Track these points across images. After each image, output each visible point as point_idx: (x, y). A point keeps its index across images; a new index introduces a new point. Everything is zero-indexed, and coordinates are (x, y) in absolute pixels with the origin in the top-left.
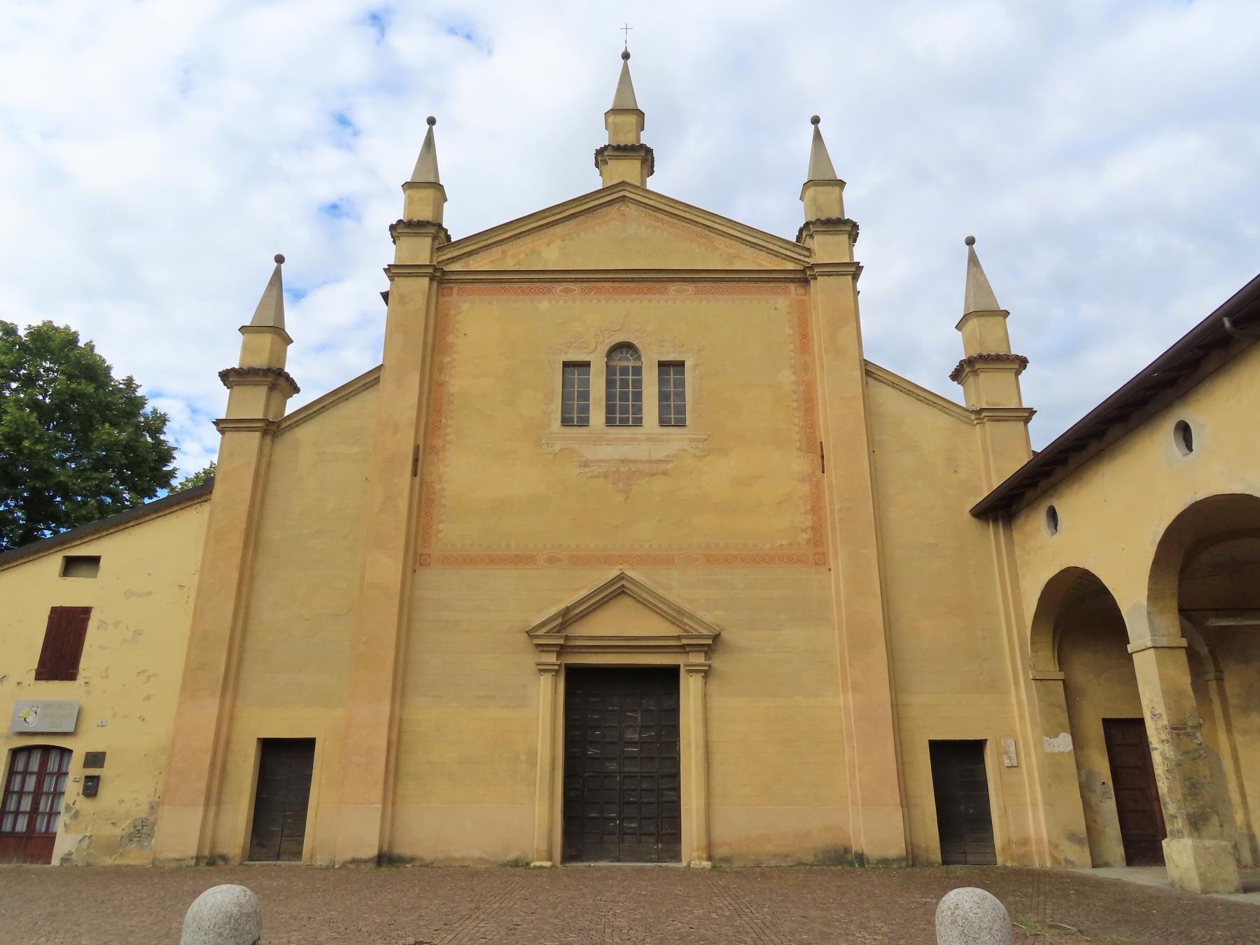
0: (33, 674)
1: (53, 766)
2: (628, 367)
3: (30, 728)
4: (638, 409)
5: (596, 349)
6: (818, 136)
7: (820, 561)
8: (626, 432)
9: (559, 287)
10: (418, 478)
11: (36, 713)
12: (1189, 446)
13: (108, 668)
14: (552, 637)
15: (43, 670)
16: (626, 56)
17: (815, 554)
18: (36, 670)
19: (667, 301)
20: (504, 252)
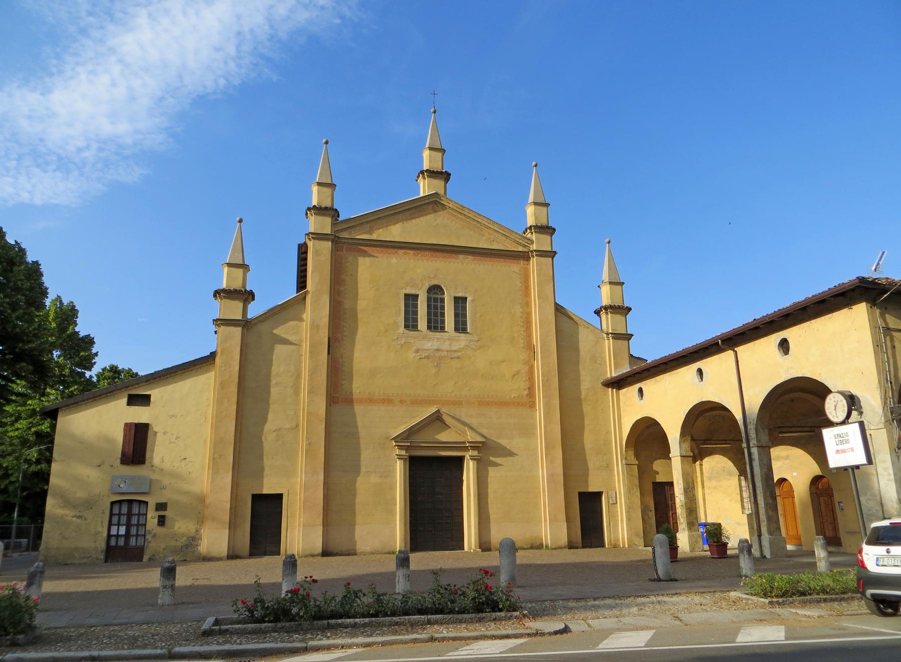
0: (119, 461)
1: (135, 510)
2: (438, 298)
3: (124, 490)
4: (443, 322)
5: (422, 287)
7: (532, 405)
8: (438, 335)
9: (401, 252)
10: (330, 355)
11: (125, 482)
12: (702, 379)
13: (163, 457)
14: (404, 442)
17: (530, 402)
18: (357, 472)
19: (458, 263)
20: (371, 227)
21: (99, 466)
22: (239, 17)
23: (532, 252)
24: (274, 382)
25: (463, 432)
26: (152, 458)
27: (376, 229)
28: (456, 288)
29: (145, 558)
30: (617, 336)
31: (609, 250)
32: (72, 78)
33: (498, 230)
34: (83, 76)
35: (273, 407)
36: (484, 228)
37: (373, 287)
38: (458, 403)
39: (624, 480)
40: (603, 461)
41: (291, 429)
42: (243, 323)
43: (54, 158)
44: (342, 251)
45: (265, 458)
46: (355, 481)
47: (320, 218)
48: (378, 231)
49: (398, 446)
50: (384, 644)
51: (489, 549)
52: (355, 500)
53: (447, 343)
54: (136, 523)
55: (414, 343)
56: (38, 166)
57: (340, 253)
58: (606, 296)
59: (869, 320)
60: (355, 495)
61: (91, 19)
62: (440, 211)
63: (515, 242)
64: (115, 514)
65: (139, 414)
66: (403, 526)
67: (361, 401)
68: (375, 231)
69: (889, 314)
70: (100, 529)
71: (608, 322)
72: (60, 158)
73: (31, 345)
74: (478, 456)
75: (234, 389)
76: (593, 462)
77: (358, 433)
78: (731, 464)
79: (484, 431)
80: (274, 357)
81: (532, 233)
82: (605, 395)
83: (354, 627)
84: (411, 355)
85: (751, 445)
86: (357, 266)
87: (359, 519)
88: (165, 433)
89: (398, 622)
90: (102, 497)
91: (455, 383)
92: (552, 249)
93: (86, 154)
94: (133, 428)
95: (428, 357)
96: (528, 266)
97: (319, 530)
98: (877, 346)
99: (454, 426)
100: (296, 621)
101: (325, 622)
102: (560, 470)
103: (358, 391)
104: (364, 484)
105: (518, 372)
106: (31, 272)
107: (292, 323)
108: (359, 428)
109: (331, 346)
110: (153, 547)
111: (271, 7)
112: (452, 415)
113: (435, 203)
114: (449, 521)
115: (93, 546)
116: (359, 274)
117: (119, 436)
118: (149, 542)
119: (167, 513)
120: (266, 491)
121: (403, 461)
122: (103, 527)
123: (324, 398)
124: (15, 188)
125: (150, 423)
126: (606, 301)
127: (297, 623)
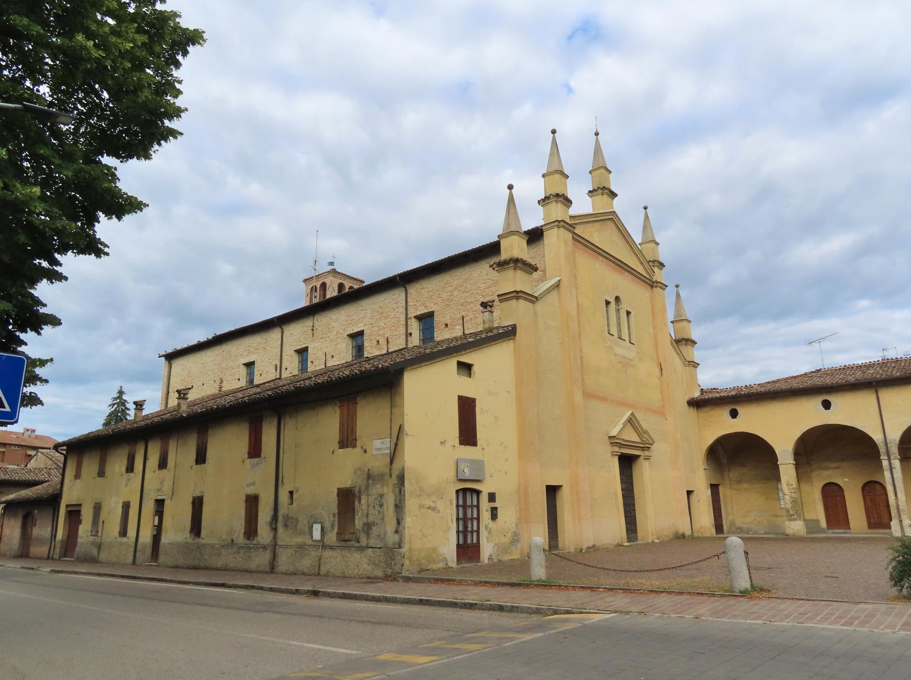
6: (647, 216)
15: (462, 438)
16: (597, 134)
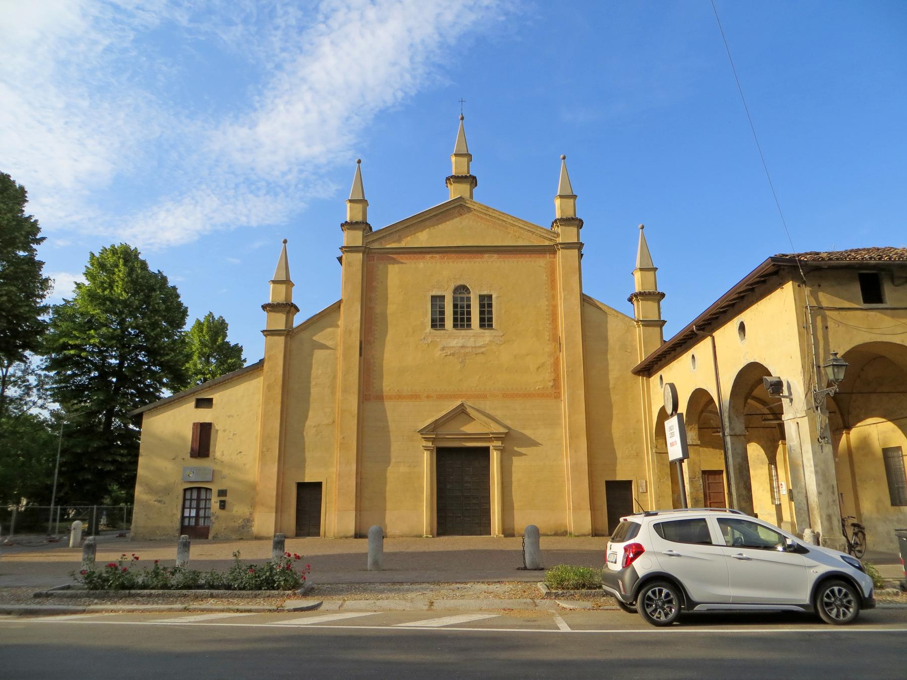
0: (189, 455)
1: (203, 496)
3: (192, 479)
4: (469, 320)
7: (558, 396)
18: (388, 462)
21: (174, 459)
22: (410, 30)
23: (557, 245)
24: (314, 384)
25: (487, 424)
26: (214, 452)
27: (404, 238)
28: (481, 287)
29: (210, 536)
30: (647, 323)
31: (643, 234)
32: (272, 110)
33: (522, 226)
34: (281, 108)
35: (313, 405)
36: (509, 226)
37: (402, 292)
38: (483, 396)
39: (653, 469)
40: (632, 449)
41: (328, 425)
42: (286, 332)
43: (264, 183)
44: (374, 260)
45: (306, 450)
46: (385, 471)
47: (352, 232)
48: (406, 239)
49: (424, 438)
50: (143, 611)
51: (513, 535)
52: (386, 488)
53: (472, 339)
54: (204, 507)
55: (440, 341)
56: (251, 192)
57: (371, 262)
58: (638, 283)
59: (795, 300)
60: (385, 484)
61: (284, 55)
62: (465, 214)
63: (541, 236)
64: (187, 499)
65: (204, 415)
66: (429, 512)
67: (390, 398)
68: (404, 240)
69: (824, 292)
70: (175, 511)
71: (639, 310)
72: (268, 184)
73: (167, 358)
74: (502, 447)
75: (278, 391)
76: (621, 451)
77: (388, 427)
78: (763, 452)
79: (508, 423)
80: (314, 361)
81: (558, 226)
82: (635, 383)
83: (150, 596)
84: (438, 353)
85: (726, 434)
86: (387, 273)
87: (389, 505)
88: (224, 431)
89: (186, 594)
90: (176, 485)
91: (480, 377)
92: (578, 239)
93: (289, 177)
94: (199, 427)
95: (453, 354)
96: (555, 260)
97: (352, 515)
98: (803, 328)
99: (478, 418)
100: (105, 589)
101: (127, 591)
102: (584, 459)
103: (388, 389)
104: (394, 474)
105: (543, 364)
106: (168, 296)
107: (329, 330)
108: (389, 423)
109: (363, 349)
110: (216, 527)
111: (439, 15)
112: (477, 407)
113: (461, 206)
114: (477, 508)
115: (171, 525)
116: (389, 280)
117: (188, 433)
118: (213, 523)
119: (228, 499)
120: (307, 480)
121: (499, 452)
122: (177, 510)
123: (356, 396)
124: (235, 214)
125: (212, 422)
126: (638, 289)
127: (105, 591)
